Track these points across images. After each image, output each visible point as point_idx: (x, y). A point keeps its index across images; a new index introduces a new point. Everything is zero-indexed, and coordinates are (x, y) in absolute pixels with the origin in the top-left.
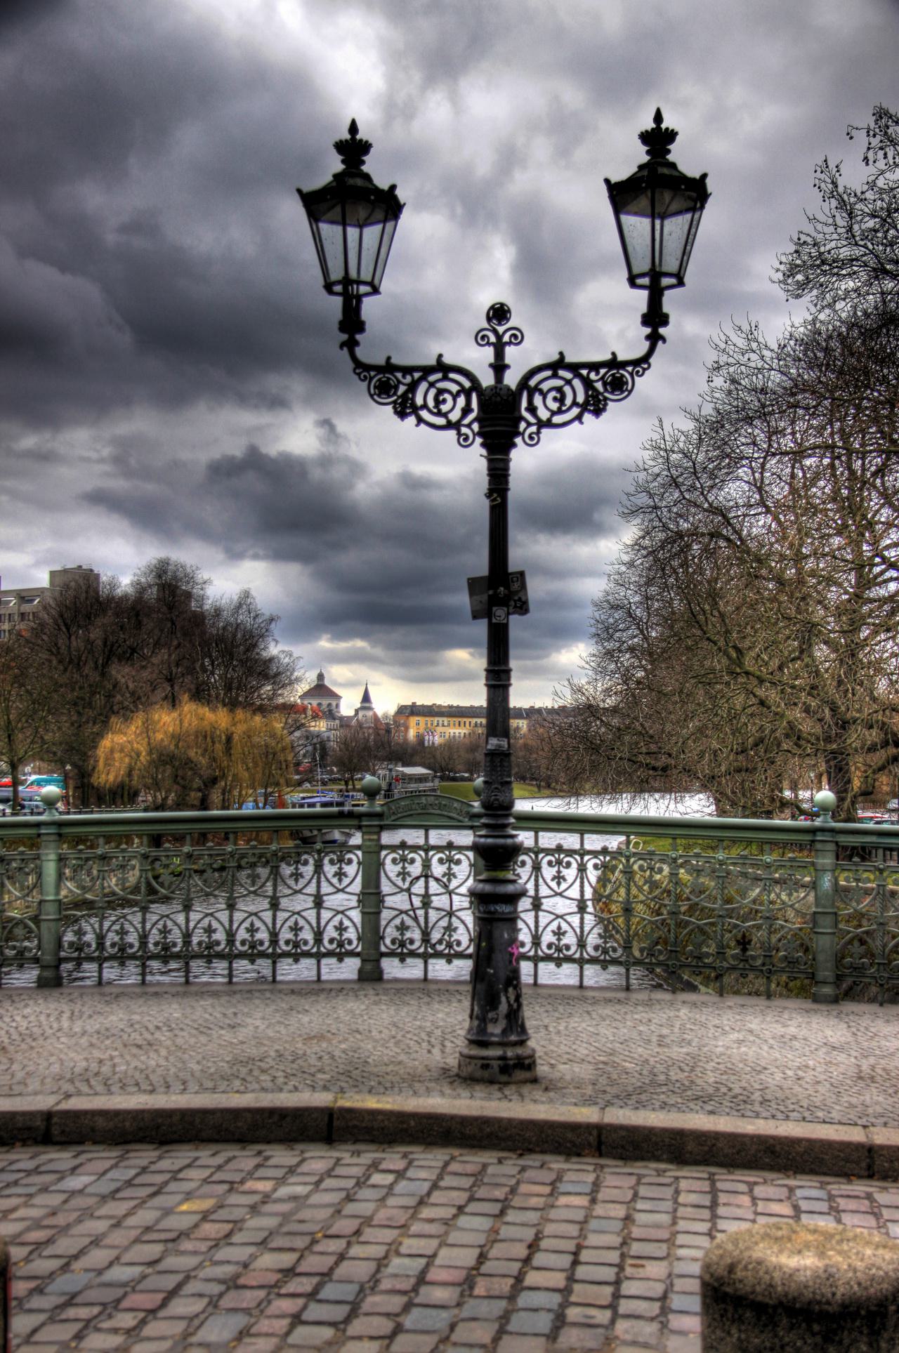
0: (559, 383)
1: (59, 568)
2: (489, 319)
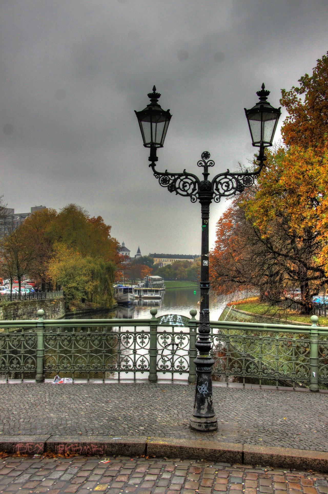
0: (226, 180)
1: (34, 206)
2: (202, 157)
